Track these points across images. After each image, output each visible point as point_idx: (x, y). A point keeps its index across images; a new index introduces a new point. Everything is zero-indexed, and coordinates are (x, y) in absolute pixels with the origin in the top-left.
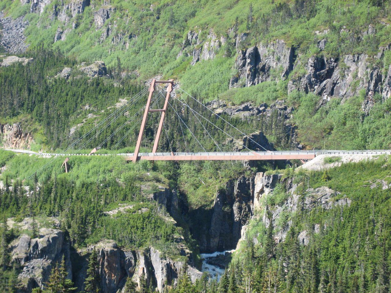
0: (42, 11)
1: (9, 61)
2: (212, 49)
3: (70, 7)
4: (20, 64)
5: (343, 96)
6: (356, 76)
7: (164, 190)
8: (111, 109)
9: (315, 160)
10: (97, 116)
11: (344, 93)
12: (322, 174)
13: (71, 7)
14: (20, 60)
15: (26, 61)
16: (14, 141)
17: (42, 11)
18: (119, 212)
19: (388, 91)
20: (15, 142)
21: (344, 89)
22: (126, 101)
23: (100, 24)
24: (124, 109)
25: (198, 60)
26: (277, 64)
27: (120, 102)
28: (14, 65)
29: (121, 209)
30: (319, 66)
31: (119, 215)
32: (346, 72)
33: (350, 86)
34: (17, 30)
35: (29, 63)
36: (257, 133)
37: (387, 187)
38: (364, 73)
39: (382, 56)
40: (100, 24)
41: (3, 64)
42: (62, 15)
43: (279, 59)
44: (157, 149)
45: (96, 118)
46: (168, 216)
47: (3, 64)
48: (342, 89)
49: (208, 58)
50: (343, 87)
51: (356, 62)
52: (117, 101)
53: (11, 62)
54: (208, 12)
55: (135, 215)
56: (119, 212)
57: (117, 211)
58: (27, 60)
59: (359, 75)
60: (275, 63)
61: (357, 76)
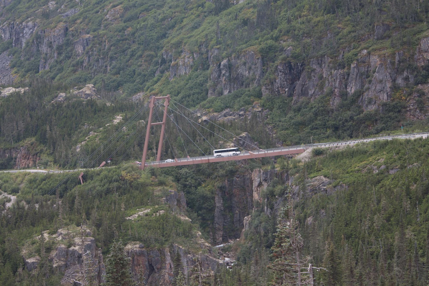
0: (24, 45)
1: (7, 92)
2: (187, 65)
3: (50, 39)
4: (18, 94)
5: (312, 95)
6: (321, 77)
7: (173, 193)
8: (109, 126)
9: (305, 154)
10: (98, 134)
11: (313, 92)
12: (427, 159)
13: (51, 39)
14: (17, 90)
15: (22, 90)
16: (23, 162)
17: (24, 45)
18: (139, 216)
19: (352, 88)
20: (24, 164)
21: (312, 89)
22: (121, 118)
23: (80, 52)
24: (120, 124)
25: (175, 75)
26: (249, 72)
27: (116, 119)
28: (12, 95)
29: (141, 213)
30: (287, 71)
31: (140, 218)
32: (312, 74)
33: (317, 86)
34: (3, 63)
35: (25, 92)
36: (244, 134)
37: (377, 172)
38: (329, 73)
39: (268, 40)
40: (80, 52)
41: (3, 95)
42: (44, 46)
43: (250, 68)
44: (161, 156)
45: (97, 135)
46: (183, 216)
47: (3, 95)
48: (311, 90)
49: (183, 73)
50: (311, 88)
51: (320, 65)
52: (113, 119)
53: (9, 93)
54: (178, 33)
55: (153, 217)
56: (139, 216)
57: (137, 215)
58: (23, 89)
59: (324, 76)
60: (247, 72)
61: (322, 77)
